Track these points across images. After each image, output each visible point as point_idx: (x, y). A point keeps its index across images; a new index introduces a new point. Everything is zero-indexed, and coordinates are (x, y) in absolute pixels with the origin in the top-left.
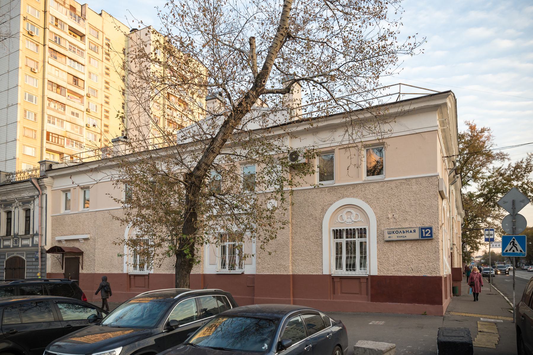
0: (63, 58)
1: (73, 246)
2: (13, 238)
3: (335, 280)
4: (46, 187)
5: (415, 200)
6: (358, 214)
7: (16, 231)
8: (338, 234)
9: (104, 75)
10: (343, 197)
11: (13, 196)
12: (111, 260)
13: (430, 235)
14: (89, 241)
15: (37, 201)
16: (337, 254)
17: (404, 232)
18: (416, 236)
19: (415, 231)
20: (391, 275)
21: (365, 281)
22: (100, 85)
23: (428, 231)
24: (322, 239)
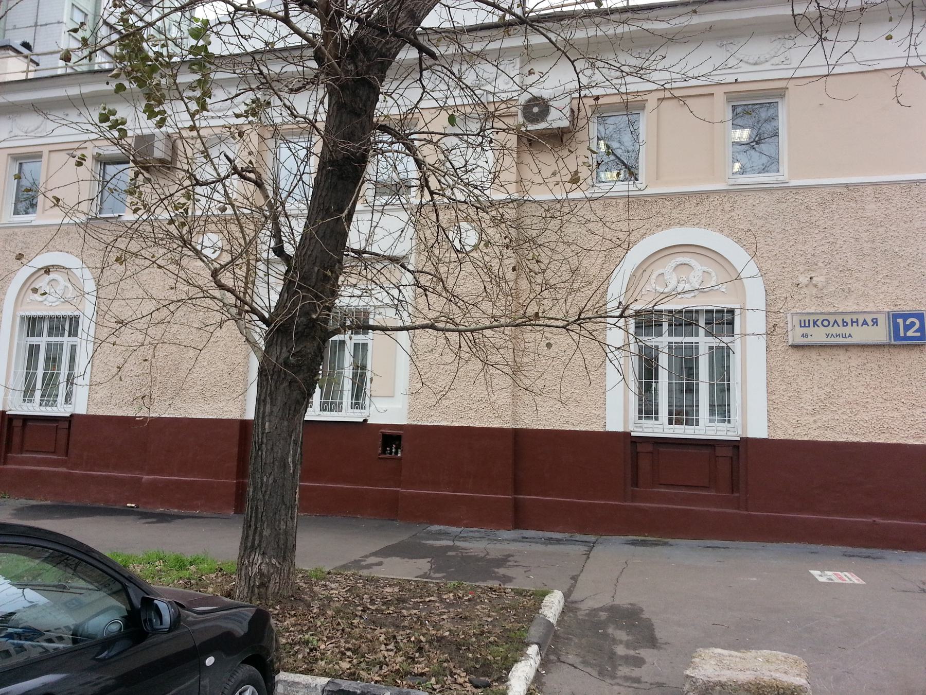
3: (640, 448)
6: (710, 270)
10: (669, 226)
13: (918, 334)
17: (845, 324)
18: (880, 334)
19: (875, 322)
20: (806, 438)
21: (729, 452)
23: (913, 324)
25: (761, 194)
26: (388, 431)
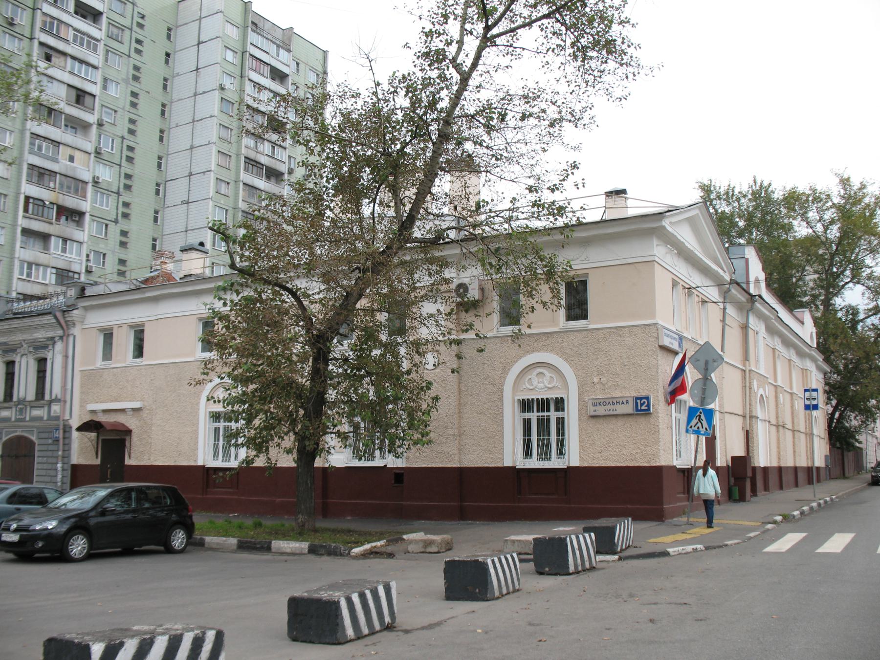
0: (62, 58)
1: (115, 420)
2: (16, 406)
4: (74, 324)
5: (628, 358)
6: (553, 376)
7: (22, 394)
8: (526, 406)
9: (131, 80)
11: (19, 337)
12: (178, 443)
14: (141, 413)
15: (59, 346)
16: (524, 435)
18: (629, 409)
19: (627, 402)
20: (597, 465)
21: (55, 474)
22: (118, 93)
23: (644, 402)
24: (502, 412)
25: (576, 333)
26: (397, 471)
